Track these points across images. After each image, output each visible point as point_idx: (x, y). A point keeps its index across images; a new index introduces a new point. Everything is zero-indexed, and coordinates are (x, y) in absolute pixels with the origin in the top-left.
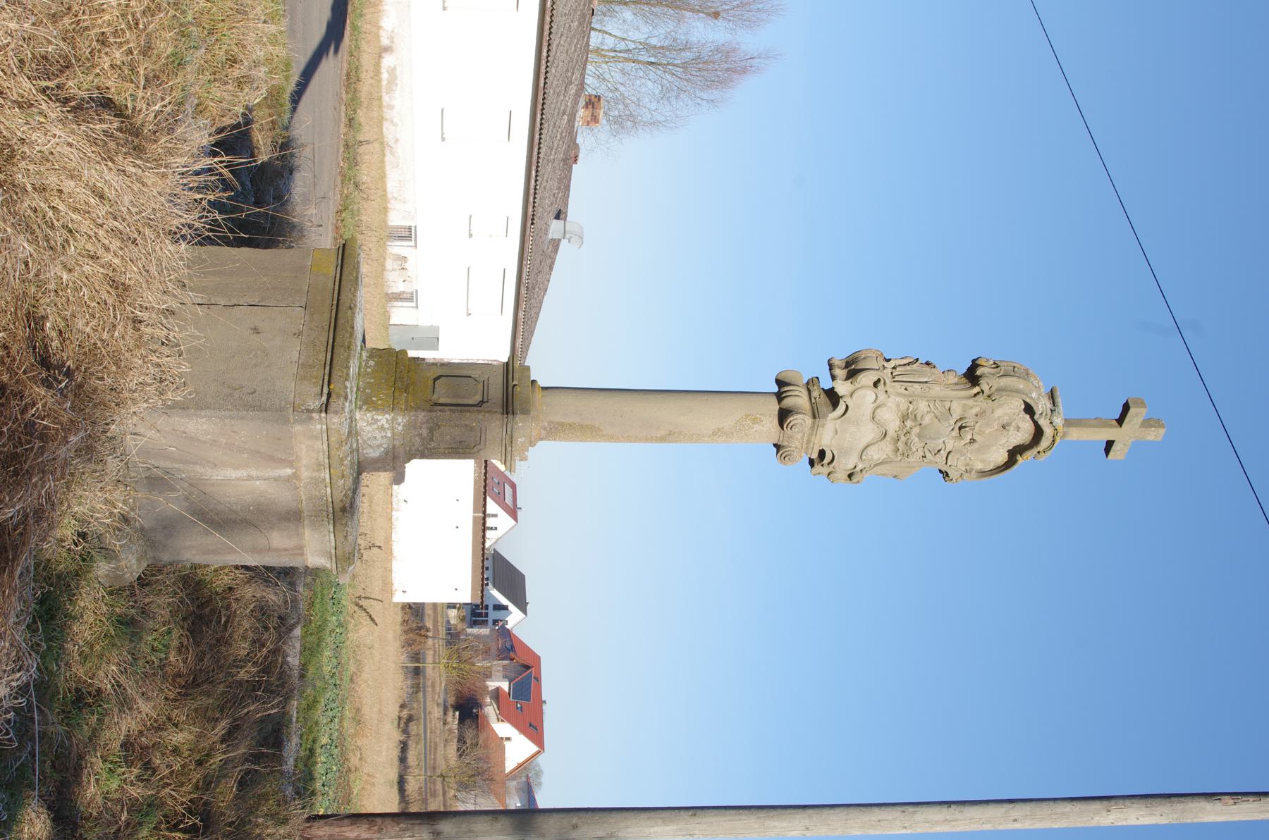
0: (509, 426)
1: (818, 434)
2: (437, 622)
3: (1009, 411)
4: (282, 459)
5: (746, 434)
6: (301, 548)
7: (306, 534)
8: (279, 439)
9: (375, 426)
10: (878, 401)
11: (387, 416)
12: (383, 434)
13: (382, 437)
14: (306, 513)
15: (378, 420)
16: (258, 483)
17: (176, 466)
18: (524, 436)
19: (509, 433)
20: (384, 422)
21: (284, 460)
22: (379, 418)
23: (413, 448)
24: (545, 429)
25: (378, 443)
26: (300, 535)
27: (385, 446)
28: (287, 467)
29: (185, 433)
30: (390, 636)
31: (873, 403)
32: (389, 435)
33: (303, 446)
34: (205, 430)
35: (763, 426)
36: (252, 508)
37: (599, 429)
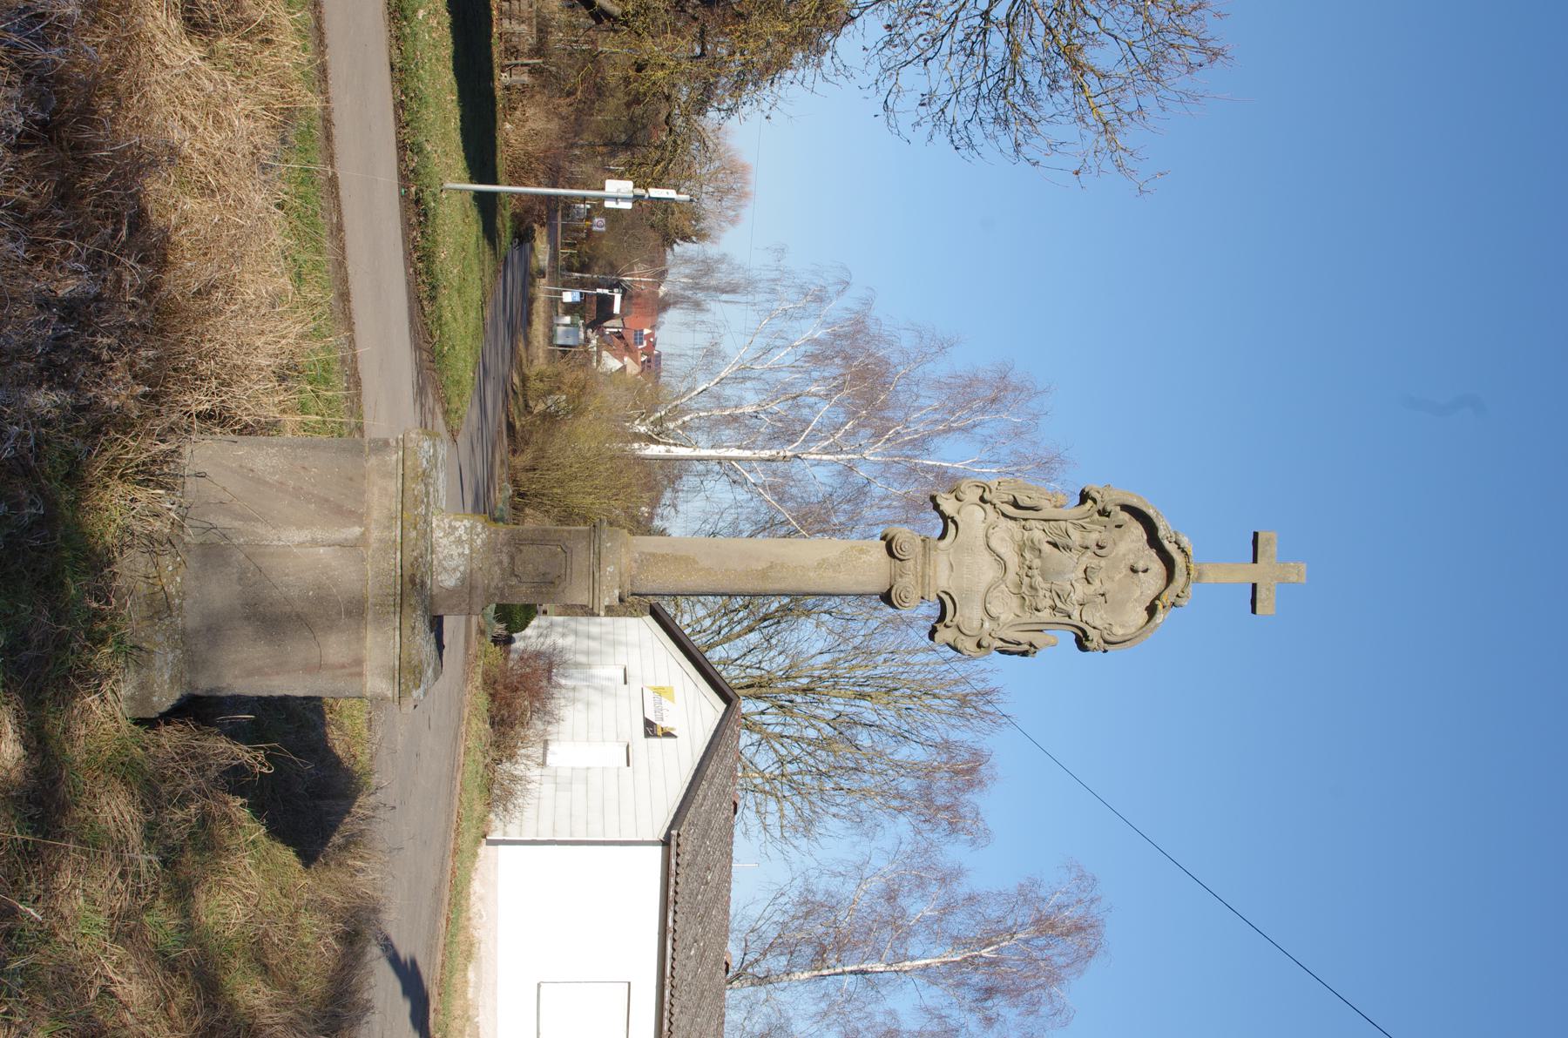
0: (597, 541)
1: (932, 562)
2: (509, 436)
3: (1132, 546)
4: (351, 511)
5: (854, 567)
6: (359, 662)
7: (368, 636)
8: (351, 479)
9: (452, 538)
10: (988, 521)
11: (466, 522)
12: (460, 550)
13: (459, 555)
14: (371, 600)
15: (455, 529)
16: (322, 550)
17: (237, 524)
18: (614, 564)
19: (597, 550)
20: (461, 531)
21: (351, 512)
22: (457, 524)
23: (493, 585)
24: (636, 562)
25: (453, 564)
26: (361, 640)
27: (462, 568)
28: (354, 524)
29: (252, 471)
30: (450, 43)
31: (983, 522)
32: (467, 552)
33: (376, 490)
34: (273, 467)
35: (871, 556)
36: (311, 593)
37: (694, 560)
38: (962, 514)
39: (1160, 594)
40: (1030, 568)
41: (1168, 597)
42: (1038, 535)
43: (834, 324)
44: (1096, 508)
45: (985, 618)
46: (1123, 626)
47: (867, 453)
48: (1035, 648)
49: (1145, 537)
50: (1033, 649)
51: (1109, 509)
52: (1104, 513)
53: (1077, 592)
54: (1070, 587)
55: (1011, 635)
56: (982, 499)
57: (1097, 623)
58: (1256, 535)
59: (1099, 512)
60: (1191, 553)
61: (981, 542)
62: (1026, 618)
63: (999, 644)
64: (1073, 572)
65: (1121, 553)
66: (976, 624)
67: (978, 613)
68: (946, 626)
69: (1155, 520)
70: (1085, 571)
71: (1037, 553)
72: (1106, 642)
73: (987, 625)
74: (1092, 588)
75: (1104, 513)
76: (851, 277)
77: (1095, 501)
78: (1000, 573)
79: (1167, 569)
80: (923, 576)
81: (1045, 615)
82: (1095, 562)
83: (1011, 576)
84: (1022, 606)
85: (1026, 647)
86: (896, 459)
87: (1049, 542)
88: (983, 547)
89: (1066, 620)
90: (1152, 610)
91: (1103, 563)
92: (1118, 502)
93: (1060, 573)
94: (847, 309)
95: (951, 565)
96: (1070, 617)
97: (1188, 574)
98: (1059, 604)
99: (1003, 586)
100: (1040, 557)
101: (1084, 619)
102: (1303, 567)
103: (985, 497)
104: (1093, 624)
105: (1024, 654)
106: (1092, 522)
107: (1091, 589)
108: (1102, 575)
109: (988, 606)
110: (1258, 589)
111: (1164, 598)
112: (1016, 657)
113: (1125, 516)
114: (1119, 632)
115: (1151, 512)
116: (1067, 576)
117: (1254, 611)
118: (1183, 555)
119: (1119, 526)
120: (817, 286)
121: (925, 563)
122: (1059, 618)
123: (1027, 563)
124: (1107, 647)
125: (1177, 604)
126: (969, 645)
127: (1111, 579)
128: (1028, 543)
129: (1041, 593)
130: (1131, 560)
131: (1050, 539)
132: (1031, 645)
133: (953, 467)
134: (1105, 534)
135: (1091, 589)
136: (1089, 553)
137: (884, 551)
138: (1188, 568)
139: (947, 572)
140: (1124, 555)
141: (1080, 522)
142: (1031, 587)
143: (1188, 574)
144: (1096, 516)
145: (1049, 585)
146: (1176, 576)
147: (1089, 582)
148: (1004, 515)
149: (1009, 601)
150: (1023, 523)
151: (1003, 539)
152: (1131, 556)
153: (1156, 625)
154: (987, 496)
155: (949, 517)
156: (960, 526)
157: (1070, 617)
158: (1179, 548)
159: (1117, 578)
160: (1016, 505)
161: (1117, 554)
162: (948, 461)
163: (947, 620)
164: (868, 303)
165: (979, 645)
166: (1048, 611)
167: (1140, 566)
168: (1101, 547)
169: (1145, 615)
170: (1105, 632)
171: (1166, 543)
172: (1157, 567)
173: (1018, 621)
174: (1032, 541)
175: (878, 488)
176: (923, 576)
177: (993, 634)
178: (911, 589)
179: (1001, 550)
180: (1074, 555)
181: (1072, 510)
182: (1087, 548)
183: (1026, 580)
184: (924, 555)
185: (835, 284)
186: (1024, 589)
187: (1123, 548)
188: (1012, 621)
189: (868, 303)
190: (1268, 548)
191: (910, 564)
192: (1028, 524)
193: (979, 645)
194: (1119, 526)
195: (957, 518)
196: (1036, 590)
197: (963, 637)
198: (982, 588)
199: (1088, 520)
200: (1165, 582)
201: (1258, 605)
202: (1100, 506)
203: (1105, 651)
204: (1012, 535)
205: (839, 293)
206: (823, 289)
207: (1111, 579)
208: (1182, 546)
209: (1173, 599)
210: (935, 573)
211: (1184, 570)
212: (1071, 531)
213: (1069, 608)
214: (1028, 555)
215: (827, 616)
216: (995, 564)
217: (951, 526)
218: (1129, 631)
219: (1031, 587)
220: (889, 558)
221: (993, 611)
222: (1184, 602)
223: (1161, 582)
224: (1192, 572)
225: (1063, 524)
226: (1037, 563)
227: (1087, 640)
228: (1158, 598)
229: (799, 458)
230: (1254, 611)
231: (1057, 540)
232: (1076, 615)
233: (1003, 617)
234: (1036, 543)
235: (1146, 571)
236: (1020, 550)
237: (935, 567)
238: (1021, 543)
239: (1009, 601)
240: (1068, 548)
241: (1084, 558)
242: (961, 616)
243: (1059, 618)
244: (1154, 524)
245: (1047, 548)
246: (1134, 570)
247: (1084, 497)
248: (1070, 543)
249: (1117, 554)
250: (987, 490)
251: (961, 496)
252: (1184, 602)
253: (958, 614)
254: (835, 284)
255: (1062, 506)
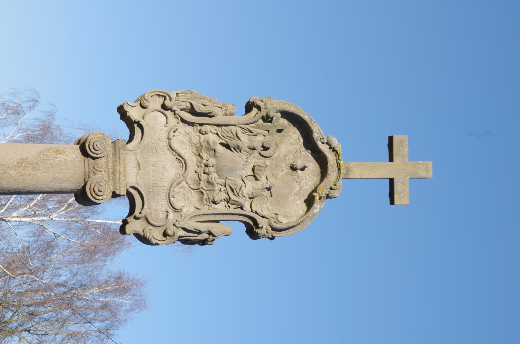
3: (291, 148)
10: (170, 125)
38: (147, 118)
39: (316, 188)
40: (207, 166)
41: (323, 190)
42: (212, 138)
43: (27, 130)
44: (260, 114)
45: (170, 210)
46: (286, 216)
47: (53, 216)
48: (214, 236)
49: (302, 140)
50: (211, 237)
51: (271, 115)
52: (267, 119)
53: (247, 187)
54: (241, 182)
55: (192, 225)
56: (164, 107)
57: (265, 213)
58: (391, 139)
59: (263, 118)
60: (339, 148)
61: (164, 143)
62: (205, 210)
63: (182, 233)
64: (243, 169)
65: (282, 154)
66: (162, 215)
67: (164, 206)
68: (136, 218)
69: (310, 124)
70: (253, 170)
71: (213, 152)
72: (274, 229)
73: (171, 216)
74: (260, 183)
75: (267, 119)
76: (39, 97)
77: (259, 108)
78: (181, 171)
79: (321, 167)
80: (114, 173)
81: (221, 207)
82: (261, 161)
83: (191, 174)
84: (201, 200)
85: (205, 236)
86: (74, 219)
87: (222, 144)
88: (166, 147)
89: (239, 211)
90: (310, 202)
91: (268, 162)
92: (278, 109)
93: (233, 170)
94: (36, 119)
95: (139, 164)
96: (242, 208)
97: (339, 169)
98: (233, 197)
99: (184, 183)
100: (215, 156)
101: (254, 209)
102: (430, 164)
103: (166, 104)
104: (262, 214)
105: (204, 242)
106: (258, 127)
107: (259, 185)
108: (267, 172)
109: (172, 199)
110: (395, 183)
111: (320, 190)
112: (197, 246)
113: (284, 122)
114: (285, 222)
115: (306, 117)
116: (239, 173)
117: (392, 202)
118: (334, 154)
119: (280, 131)
120: (15, 104)
121: (115, 162)
122: (233, 209)
123: (204, 161)
124: (276, 234)
125: (330, 195)
126: (155, 235)
127: (275, 176)
128: (205, 145)
129: (217, 187)
130: (291, 160)
131: (223, 141)
132: (210, 233)
133: (114, 224)
134: (268, 138)
135: (259, 185)
136: (256, 153)
137: (79, 151)
138: (338, 165)
139: (135, 170)
140: (285, 156)
141: (247, 126)
142: (209, 182)
143: (339, 169)
144: (261, 121)
145: (223, 181)
146: (329, 171)
147: (257, 179)
148: (183, 121)
149: (189, 196)
150: (199, 128)
151: (183, 143)
152: (291, 157)
153: (314, 214)
154: (168, 103)
155: (135, 122)
156: (146, 129)
157: (242, 208)
158: (330, 148)
159: (279, 176)
160: (193, 112)
161: (279, 155)
162: (111, 220)
163: (137, 213)
164: (51, 115)
165: (165, 234)
166: (223, 203)
167: (299, 164)
168: (265, 148)
169: (304, 207)
170: (272, 221)
171: (319, 144)
172: (313, 166)
173: (198, 212)
174: (208, 143)
175: (61, 242)
176: (114, 173)
177: (177, 224)
178: (103, 183)
179: (182, 152)
180: (244, 155)
181: (241, 118)
182: (254, 149)
183: (204, 177)
184: (114, 154)
185: (27, 101)
186: (202, 184)
187: (283, 150)
188: (192, 213)
189: (51, 115)
190: (401, 148)
191: (102, 162)
192: (203, 128)
193: (165, 234)
194: (280, 131)
195: (142, 123)
196: (213, 184)
197: (151, 227)
198: (166, 184)
199: (254, 125)
200: (319, 178)
201: (396, 197)
202: (264, 113)
203: (272, 238)
204: (190, 139)
205: (31, 108)
206: (19, 105)
207: (275, 176)
208: (333, 146)
209: (327, 191)
210: (125, 170)
211: (335, 166)
212: (240, 134)
213: (241, 200)
214: (204, 155)
215: (27, 333)
216: (176, 163)
217: (137, 130)
218: (291, 220)
219: (209, 182)
220: (83, 157)
221: (177, 204)
222: (336, 193)
223: (317, 178)
224: (342, 168)
225: (233, 128)
226: (212, 161)
227: (258, 227)
228: (315, 190)
229: (4, 220)
230: (392, 202)
231: (231, 143)
232: (247, 207)
233: (185, 210)
234: (211, 144)
235: (303, 169)
236: (198, 151)
237: (125, 165)
238: (198, 145)
239: (189, 196)
240: (238, 149)
241: (252, 158)
242: (149, 208)
243: (233, 209)
244: (309, 127)
245: (221, 149)
246: (293, 168)
247: (249, 107)
248: (240, 143)
249: (279, 155)
250: (168, 98)
251: (146, 104)
252: (336, 193)
253: (145, 207)
254: (27, 101)
255: (232, 114)
